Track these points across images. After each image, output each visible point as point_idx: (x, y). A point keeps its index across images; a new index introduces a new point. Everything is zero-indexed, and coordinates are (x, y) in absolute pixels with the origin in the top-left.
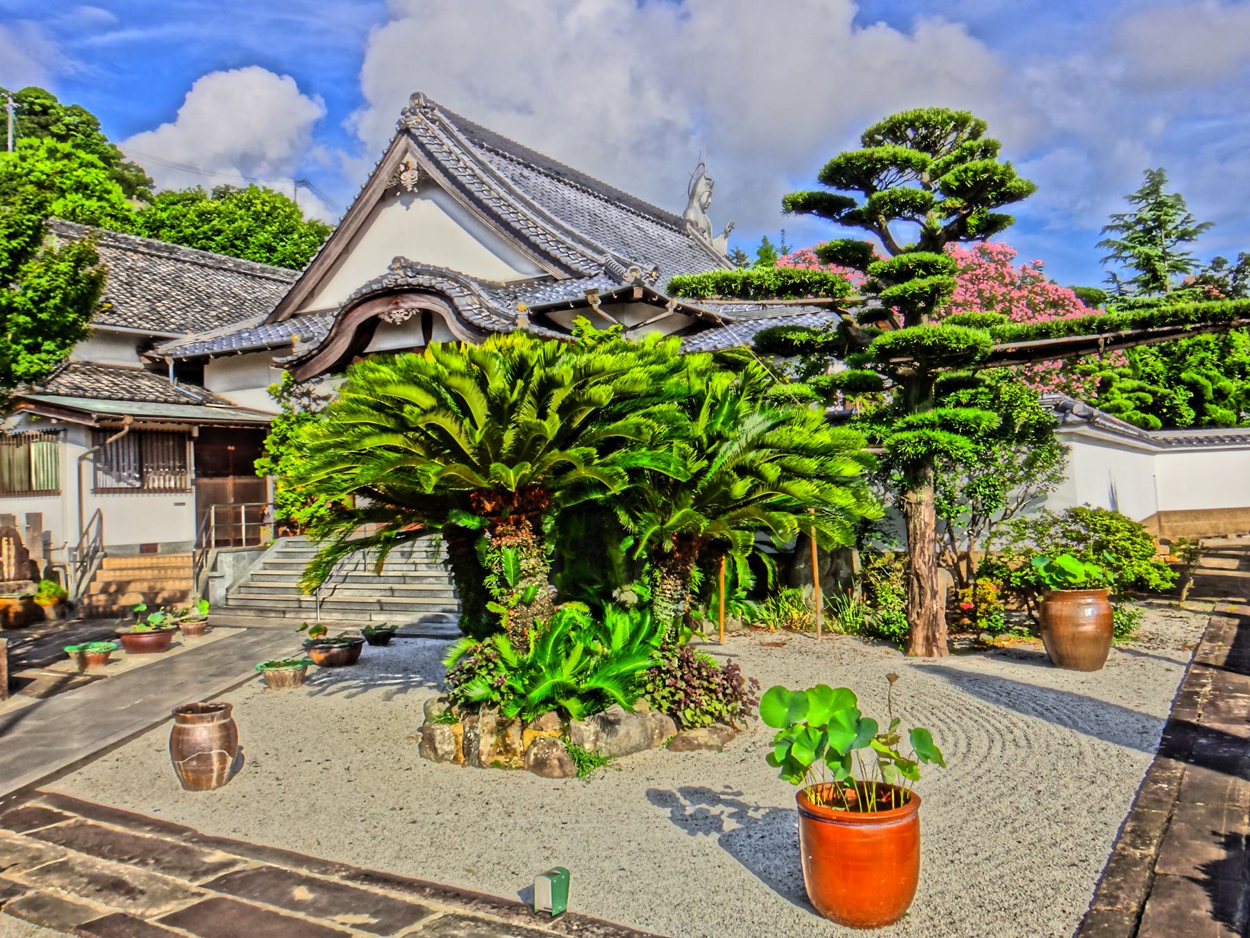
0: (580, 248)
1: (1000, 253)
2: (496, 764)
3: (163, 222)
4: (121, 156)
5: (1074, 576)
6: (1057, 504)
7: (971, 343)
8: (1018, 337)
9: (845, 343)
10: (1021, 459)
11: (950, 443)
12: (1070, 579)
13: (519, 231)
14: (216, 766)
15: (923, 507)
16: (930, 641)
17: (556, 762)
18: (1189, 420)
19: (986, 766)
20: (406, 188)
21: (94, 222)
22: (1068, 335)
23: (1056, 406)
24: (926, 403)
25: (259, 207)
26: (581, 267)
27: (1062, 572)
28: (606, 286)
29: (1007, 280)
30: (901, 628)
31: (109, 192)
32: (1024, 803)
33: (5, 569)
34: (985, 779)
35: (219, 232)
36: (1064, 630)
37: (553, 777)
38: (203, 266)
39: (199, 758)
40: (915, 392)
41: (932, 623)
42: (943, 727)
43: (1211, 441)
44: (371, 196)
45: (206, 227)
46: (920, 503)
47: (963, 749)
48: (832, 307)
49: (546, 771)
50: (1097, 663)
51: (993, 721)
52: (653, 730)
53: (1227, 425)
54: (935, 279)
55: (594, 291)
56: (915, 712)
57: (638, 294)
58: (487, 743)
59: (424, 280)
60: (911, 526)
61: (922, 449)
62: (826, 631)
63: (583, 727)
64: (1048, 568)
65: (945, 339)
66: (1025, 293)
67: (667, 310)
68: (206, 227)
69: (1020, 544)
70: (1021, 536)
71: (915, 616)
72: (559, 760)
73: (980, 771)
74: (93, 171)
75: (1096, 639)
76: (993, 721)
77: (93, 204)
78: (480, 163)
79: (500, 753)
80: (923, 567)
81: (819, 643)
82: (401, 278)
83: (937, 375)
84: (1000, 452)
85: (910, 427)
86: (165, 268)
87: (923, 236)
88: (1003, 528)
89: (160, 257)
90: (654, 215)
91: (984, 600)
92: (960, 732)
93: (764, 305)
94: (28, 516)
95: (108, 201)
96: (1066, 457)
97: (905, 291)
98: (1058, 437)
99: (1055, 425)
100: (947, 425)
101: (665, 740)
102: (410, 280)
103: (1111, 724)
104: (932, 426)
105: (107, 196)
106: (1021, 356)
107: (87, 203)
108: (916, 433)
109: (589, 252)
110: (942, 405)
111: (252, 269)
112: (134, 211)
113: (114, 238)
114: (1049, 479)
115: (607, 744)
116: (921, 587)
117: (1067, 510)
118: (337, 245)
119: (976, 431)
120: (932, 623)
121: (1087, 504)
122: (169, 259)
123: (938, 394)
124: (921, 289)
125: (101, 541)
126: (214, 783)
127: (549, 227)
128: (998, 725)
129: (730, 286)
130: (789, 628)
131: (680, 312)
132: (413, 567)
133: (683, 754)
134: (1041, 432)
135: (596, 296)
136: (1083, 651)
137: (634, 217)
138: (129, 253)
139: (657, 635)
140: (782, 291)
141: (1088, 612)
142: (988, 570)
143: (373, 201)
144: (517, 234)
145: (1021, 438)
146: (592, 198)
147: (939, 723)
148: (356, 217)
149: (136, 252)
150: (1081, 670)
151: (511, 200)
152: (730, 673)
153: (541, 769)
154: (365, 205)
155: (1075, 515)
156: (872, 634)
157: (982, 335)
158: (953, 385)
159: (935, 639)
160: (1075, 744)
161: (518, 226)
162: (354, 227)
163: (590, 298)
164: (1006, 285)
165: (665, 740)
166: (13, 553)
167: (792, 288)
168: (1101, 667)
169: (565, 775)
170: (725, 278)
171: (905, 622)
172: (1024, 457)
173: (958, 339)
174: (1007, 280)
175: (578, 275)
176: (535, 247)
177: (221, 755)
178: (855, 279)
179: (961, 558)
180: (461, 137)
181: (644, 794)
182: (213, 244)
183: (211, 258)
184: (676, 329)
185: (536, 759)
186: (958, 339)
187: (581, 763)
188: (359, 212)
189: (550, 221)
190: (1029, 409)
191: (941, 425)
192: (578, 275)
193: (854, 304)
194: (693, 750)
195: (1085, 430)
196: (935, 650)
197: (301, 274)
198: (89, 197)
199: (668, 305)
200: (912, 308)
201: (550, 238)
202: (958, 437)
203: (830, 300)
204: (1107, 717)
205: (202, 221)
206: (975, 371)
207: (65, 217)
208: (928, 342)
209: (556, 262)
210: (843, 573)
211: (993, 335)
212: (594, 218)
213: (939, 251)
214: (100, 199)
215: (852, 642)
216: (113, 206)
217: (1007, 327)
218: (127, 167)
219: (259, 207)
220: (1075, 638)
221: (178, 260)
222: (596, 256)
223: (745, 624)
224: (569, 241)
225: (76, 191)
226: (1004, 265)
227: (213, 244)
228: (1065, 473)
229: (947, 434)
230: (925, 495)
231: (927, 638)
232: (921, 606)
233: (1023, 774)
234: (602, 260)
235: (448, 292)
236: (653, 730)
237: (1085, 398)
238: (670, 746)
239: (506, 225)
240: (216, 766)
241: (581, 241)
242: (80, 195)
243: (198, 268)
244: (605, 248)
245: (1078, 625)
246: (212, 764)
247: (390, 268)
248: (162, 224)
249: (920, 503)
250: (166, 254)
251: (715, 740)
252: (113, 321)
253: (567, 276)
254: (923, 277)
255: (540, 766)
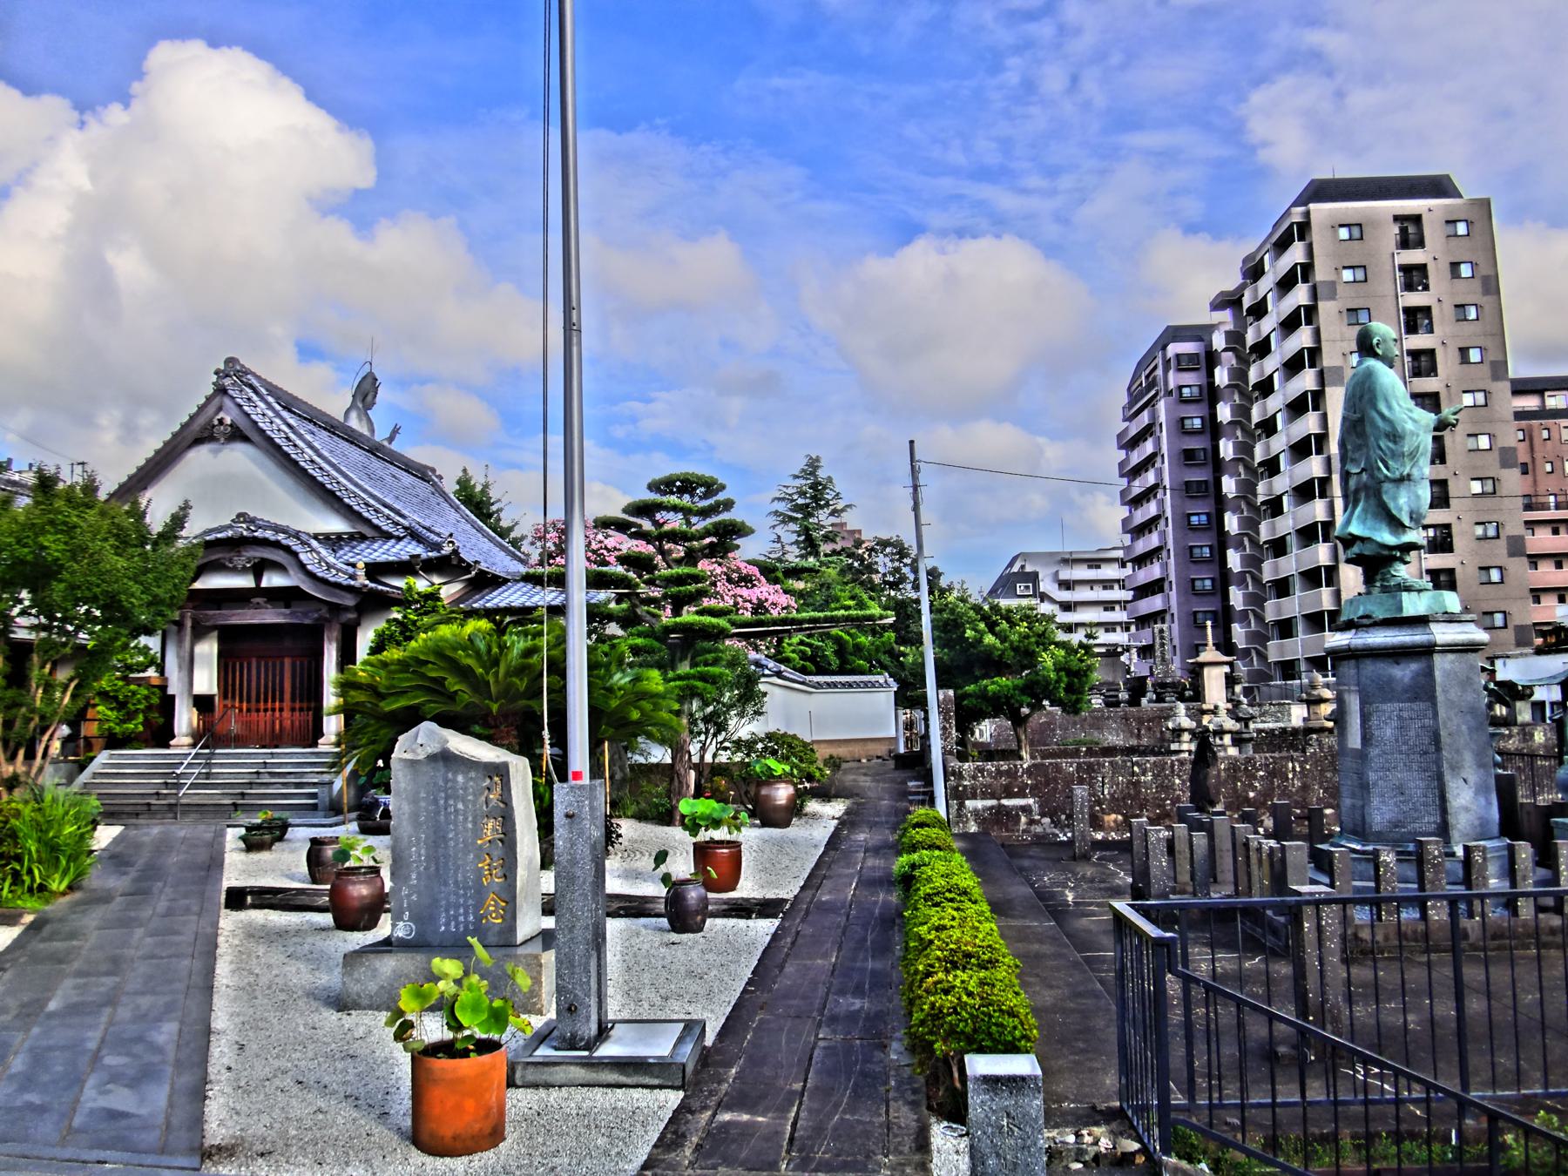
0: (387, 511)
18: (834, 667)
26: (387, 527)
43: (850, 685)
50: (787, 824)
53: (862, 673)
59: (269, 534)
78: (289, 426)
82: (243, 530)
175: (388, 536)
180: (270, 399)
209: (368, 522)
234: (406, 523)
241: (386, 506)
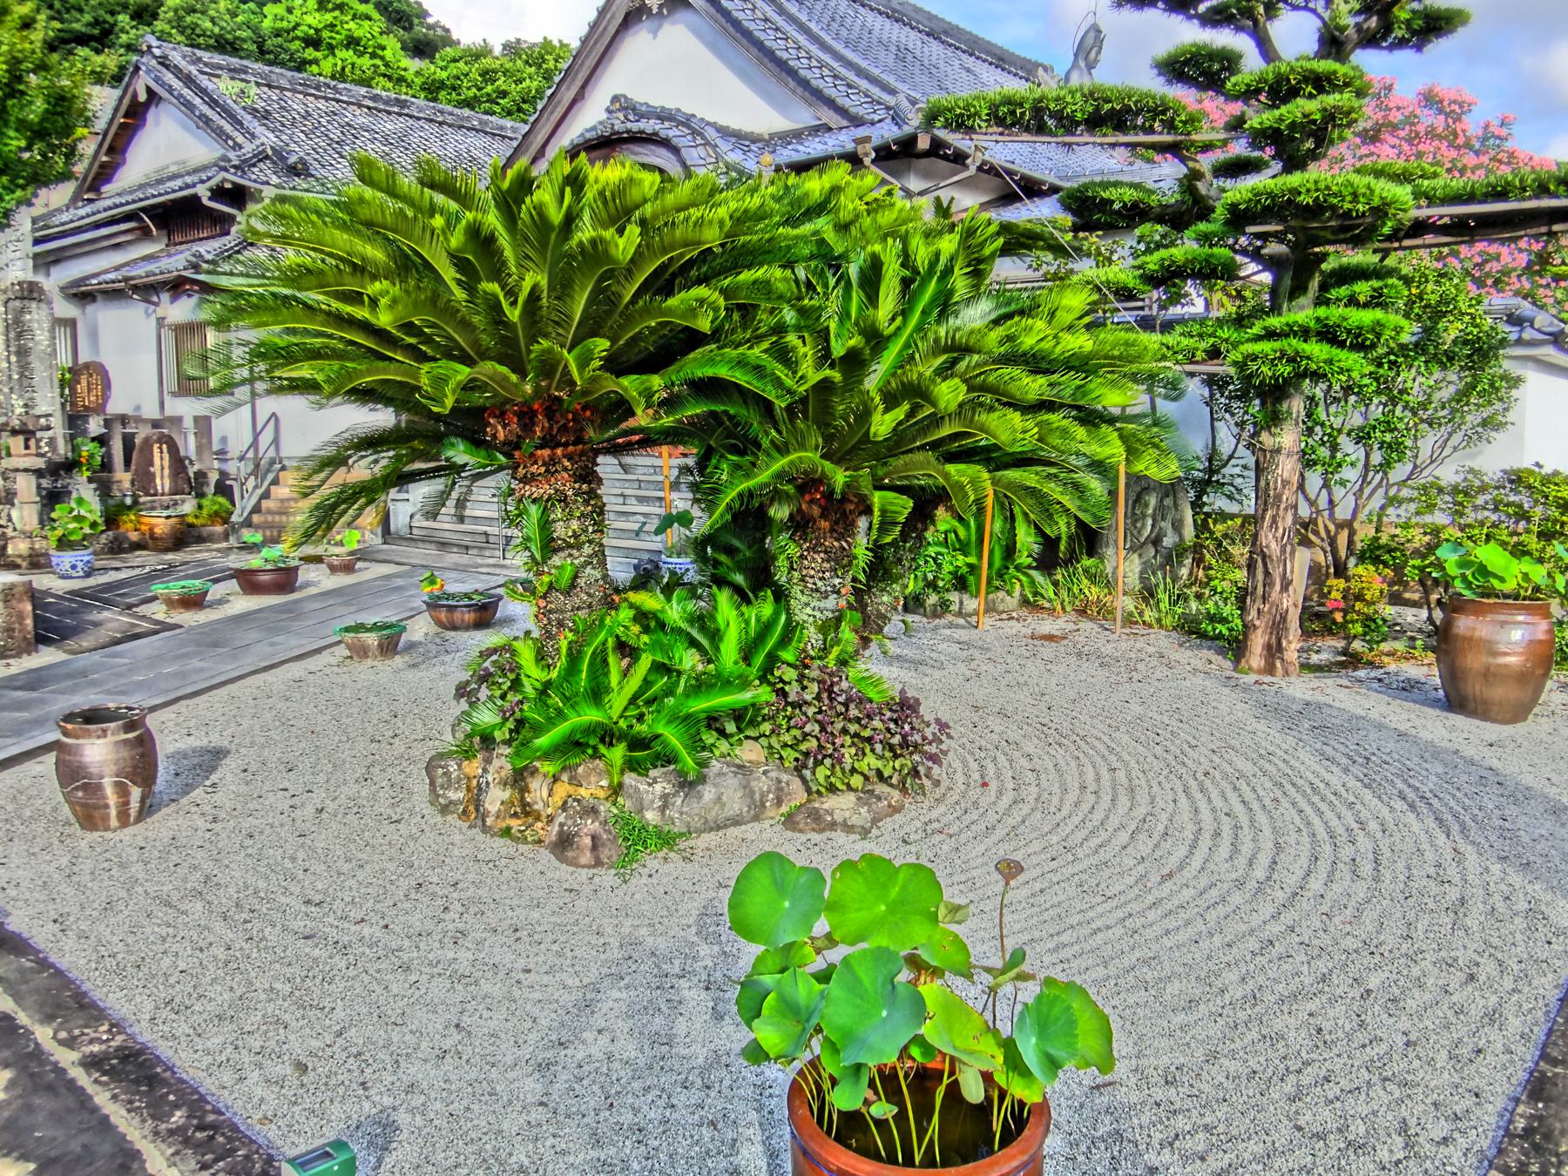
1: (1455, 102)
2: (507, 832)
3: (442, 82)
4: (425, 14)
5: (1502, 580)
6: (1493, 459)
7: (1376, 202)
8: (1457, 199)
9: (1187, 211)
10: (1447, 393)
11: (1330, 362)
12: (1495, 583)
13: (785, 62)
14: (112, 798)
15: (1282, 458)
16: (1274, 651)
17: (588, 841)
19: (1288, 918)
20: (650, 9)
21: (366, 83)
22: (1537, 196)
23: (1510, 316)
24: (1302, 300)
25: (551, 64)
27: (1483, 570)
28: (887, 132)
29: (1460, 141)
30: (1231, 630)
31: (383, 48)
32: (1338, 1017)
33: (158, 481)
34: (1279, 949)
35: (504, 94)
36: (1473, 662)
37: (578, 866)
38: (441, 123)
39: (85, 787)
40: (1287, 282)
41: (1278, 626)
42: (1244, 820)
44: (609, 22)
45: (489, 88)
46: (1278, 451)
47: (1260, 873)
48: (1173, 149)
49: (570, 854)
50: (1519, 713)
51: (1329, 815)
52: (763, 795)
54: (1331, 100)
55: (867, 139)
56: (1208, 783)
57: (923, 143)
58: (496, 798)
59: (649, 126)
60: (1262, 484)
61: (1285, 369)
62: (1129, 620)
63: (643, 787)
64: (1464, 564)
65: (1335, 195)
66: (1485, 159)
67: (966, 167)
68: (489, 88)
69: (1428, 519)
70: (1431, 507)
71: (1253, 613)
72: (594, 838)
73: (1275, 928)
74: (367, 23)
75: (1522, 677)
76: (1329, 815)
77: (365, 62)
79: (515, 815)
80: (1273, 545)
81: (1115, 643)
83: (1323, 257)
84: (1415, 380)
85: (1270, 335)
86: (389, 125)
87: (1321, 41)
88: (1405, 493)
89: (389, 113)
90: (993, 55)
91: (1359, 597)
92: (1267, 832)
93: (1070, 145)
94: (196, 419)
95: (382, 58)
96: (1514, 393)
97: (1281, 120)
98: (1506, 364)
99: (1503, 343)
100: (1328, 334)
101: (784, 809)
102: (629, 125)
103: (1525, 839)
104: (1305, 333)
105: (379, 52)
106: (1461, 229)
107: (359, 61)
108: (1277, 345)
109: (876, 91)
110: (1327, 303)
111: (502, 128)
112: (412, 71)
113: (334, 88)
114: (1484, 423)
115: (683, 811)
116: (1267, 573)
117: (1505, 472)
118: (568, 88)
119: (1373, 346)
120: (1278, 626)
121: (1537, 464)
122: (400, 115)
123: (1324, 287)
124: (1305, 116)
125: (277, 449)
126: (114, 822)
127: (827, 58)
128: (1334, 822)
129: (1013, 113)
130: (1082, 612)
131: (988, 172)
132: (620, 500)
133: (803, 838)
134: (1479, 352)
135: (868, 147)
136: (1499, 693)
137: (964, 57)
138: (352, 108)
139: (794, 644)
140: (1095, 122)
141: (1517, 635)
142: (1373, 554)
143: (612, 30)
144: (782, 65)
145: (1447, 359)
146: (907, 29)
147: (1239, 808)
148: (591, 51)
149: (360, 106)
150: (1494, 721)
151: (780, 21)
152: (905, 707)
153: (564, 849)
154: (602, 34)
155: (1516, 479)
156: (1190, 629)
157: (1403, 193)
158: (1347, 275)
159: (1280, 648)
160: (1456, 879)
161: (784, 55)
162: (590, 62)
163: (860, 150)
164: (1458, 148)
165: (784, 809)
166: (166, 463)
167: (1111, 117)
168: (1525, 719)
169: (598, 863)
170: (1008, 101)
171: (1238, 622)
172: (1452, 389)
173: (1355, 195)
174: (1460, 141)
175: (857, 121)
176: (805, 84)
177: (118, 785)
178: (1213, 110)
179: (1340, 526)
181: (955, 768)
182: (497, 109)
183: (451, 114)
184: (985, 199)
185: (561, 832)
186: (1355, 195)
187: (635, 839)
188: (596, 43)
189: (824, 46)
190: (1467, 318)
191: (1319, 334)
192: (857, 121)
193: (1207, 147)
194: (821, 831)
195: (1549, 353)
196: (1278, 665)
197: (527, 128)
198: (361, 55)
199: (969, 161)
200: (1291, 147)
201: (826, 72)
202: (1341, 354)
203: (1167, 138)
204: (1522, 820)
205: (486, 81)
206: (1386, 253)
207: (333, 77)
208: (1305, 199)
209: (831, 103)
210: (1169, 541)
211: (1417, 195)
212: (902, 54)
213: (1341, 57)
214: (373, 56)
215: (1164, 641)
216: (387, 65)
217: (1443, 182)
218: (430, 27)
219: (551, 64)
220: (1488, 675)
221: (411, 117)
222: (886, 97)
223: (1025, 602)
224: (851, 76)
225: (347, 47)
226: (1458, 119)
227: (497, 109)
228: (1510, 416)
229: (1326, 347)
230: (1288, 437)
231: (1268, 647)
232: (1264, 599)
233: (1350, 943)
235: (675, 141)
236: (763, 795)
237: (1554, 311)
238: (790, 821)
239: (770, 54)
240: (112, 798)
242: (351, 52)
243: (435, 127)
244: (899, 86)
245: (1496, 654)
246: (104, 797)
247: (609, 111)
248: (442, 85)
249: (1278, 451)
250: (396, 109)
251: (863, 816)
252: (305, 186)
253: (845, 123)
254: (1311, 96)
255: (564, 844)
